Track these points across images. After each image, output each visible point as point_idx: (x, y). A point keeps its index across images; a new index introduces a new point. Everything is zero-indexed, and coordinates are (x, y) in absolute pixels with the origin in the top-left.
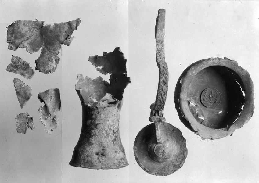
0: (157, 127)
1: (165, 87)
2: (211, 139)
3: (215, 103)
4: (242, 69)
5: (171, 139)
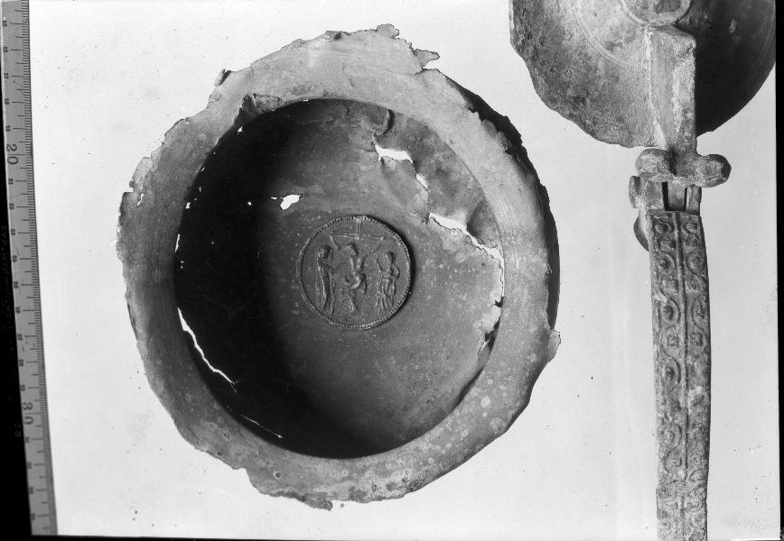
0: (686, 122)
1: (675, 352)
2: (338, 36)
3: (328, 249)
4: (220, 452)
5: (590, 51)
